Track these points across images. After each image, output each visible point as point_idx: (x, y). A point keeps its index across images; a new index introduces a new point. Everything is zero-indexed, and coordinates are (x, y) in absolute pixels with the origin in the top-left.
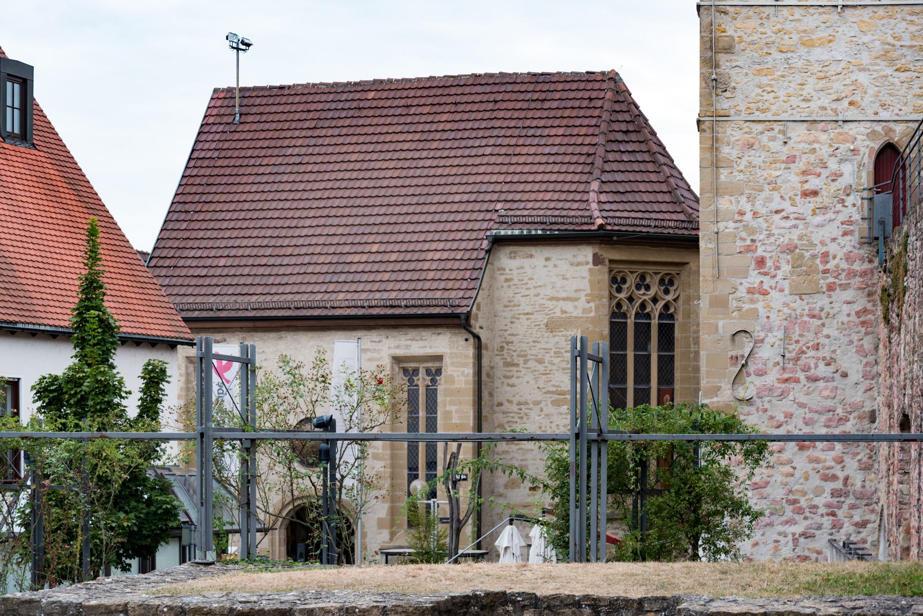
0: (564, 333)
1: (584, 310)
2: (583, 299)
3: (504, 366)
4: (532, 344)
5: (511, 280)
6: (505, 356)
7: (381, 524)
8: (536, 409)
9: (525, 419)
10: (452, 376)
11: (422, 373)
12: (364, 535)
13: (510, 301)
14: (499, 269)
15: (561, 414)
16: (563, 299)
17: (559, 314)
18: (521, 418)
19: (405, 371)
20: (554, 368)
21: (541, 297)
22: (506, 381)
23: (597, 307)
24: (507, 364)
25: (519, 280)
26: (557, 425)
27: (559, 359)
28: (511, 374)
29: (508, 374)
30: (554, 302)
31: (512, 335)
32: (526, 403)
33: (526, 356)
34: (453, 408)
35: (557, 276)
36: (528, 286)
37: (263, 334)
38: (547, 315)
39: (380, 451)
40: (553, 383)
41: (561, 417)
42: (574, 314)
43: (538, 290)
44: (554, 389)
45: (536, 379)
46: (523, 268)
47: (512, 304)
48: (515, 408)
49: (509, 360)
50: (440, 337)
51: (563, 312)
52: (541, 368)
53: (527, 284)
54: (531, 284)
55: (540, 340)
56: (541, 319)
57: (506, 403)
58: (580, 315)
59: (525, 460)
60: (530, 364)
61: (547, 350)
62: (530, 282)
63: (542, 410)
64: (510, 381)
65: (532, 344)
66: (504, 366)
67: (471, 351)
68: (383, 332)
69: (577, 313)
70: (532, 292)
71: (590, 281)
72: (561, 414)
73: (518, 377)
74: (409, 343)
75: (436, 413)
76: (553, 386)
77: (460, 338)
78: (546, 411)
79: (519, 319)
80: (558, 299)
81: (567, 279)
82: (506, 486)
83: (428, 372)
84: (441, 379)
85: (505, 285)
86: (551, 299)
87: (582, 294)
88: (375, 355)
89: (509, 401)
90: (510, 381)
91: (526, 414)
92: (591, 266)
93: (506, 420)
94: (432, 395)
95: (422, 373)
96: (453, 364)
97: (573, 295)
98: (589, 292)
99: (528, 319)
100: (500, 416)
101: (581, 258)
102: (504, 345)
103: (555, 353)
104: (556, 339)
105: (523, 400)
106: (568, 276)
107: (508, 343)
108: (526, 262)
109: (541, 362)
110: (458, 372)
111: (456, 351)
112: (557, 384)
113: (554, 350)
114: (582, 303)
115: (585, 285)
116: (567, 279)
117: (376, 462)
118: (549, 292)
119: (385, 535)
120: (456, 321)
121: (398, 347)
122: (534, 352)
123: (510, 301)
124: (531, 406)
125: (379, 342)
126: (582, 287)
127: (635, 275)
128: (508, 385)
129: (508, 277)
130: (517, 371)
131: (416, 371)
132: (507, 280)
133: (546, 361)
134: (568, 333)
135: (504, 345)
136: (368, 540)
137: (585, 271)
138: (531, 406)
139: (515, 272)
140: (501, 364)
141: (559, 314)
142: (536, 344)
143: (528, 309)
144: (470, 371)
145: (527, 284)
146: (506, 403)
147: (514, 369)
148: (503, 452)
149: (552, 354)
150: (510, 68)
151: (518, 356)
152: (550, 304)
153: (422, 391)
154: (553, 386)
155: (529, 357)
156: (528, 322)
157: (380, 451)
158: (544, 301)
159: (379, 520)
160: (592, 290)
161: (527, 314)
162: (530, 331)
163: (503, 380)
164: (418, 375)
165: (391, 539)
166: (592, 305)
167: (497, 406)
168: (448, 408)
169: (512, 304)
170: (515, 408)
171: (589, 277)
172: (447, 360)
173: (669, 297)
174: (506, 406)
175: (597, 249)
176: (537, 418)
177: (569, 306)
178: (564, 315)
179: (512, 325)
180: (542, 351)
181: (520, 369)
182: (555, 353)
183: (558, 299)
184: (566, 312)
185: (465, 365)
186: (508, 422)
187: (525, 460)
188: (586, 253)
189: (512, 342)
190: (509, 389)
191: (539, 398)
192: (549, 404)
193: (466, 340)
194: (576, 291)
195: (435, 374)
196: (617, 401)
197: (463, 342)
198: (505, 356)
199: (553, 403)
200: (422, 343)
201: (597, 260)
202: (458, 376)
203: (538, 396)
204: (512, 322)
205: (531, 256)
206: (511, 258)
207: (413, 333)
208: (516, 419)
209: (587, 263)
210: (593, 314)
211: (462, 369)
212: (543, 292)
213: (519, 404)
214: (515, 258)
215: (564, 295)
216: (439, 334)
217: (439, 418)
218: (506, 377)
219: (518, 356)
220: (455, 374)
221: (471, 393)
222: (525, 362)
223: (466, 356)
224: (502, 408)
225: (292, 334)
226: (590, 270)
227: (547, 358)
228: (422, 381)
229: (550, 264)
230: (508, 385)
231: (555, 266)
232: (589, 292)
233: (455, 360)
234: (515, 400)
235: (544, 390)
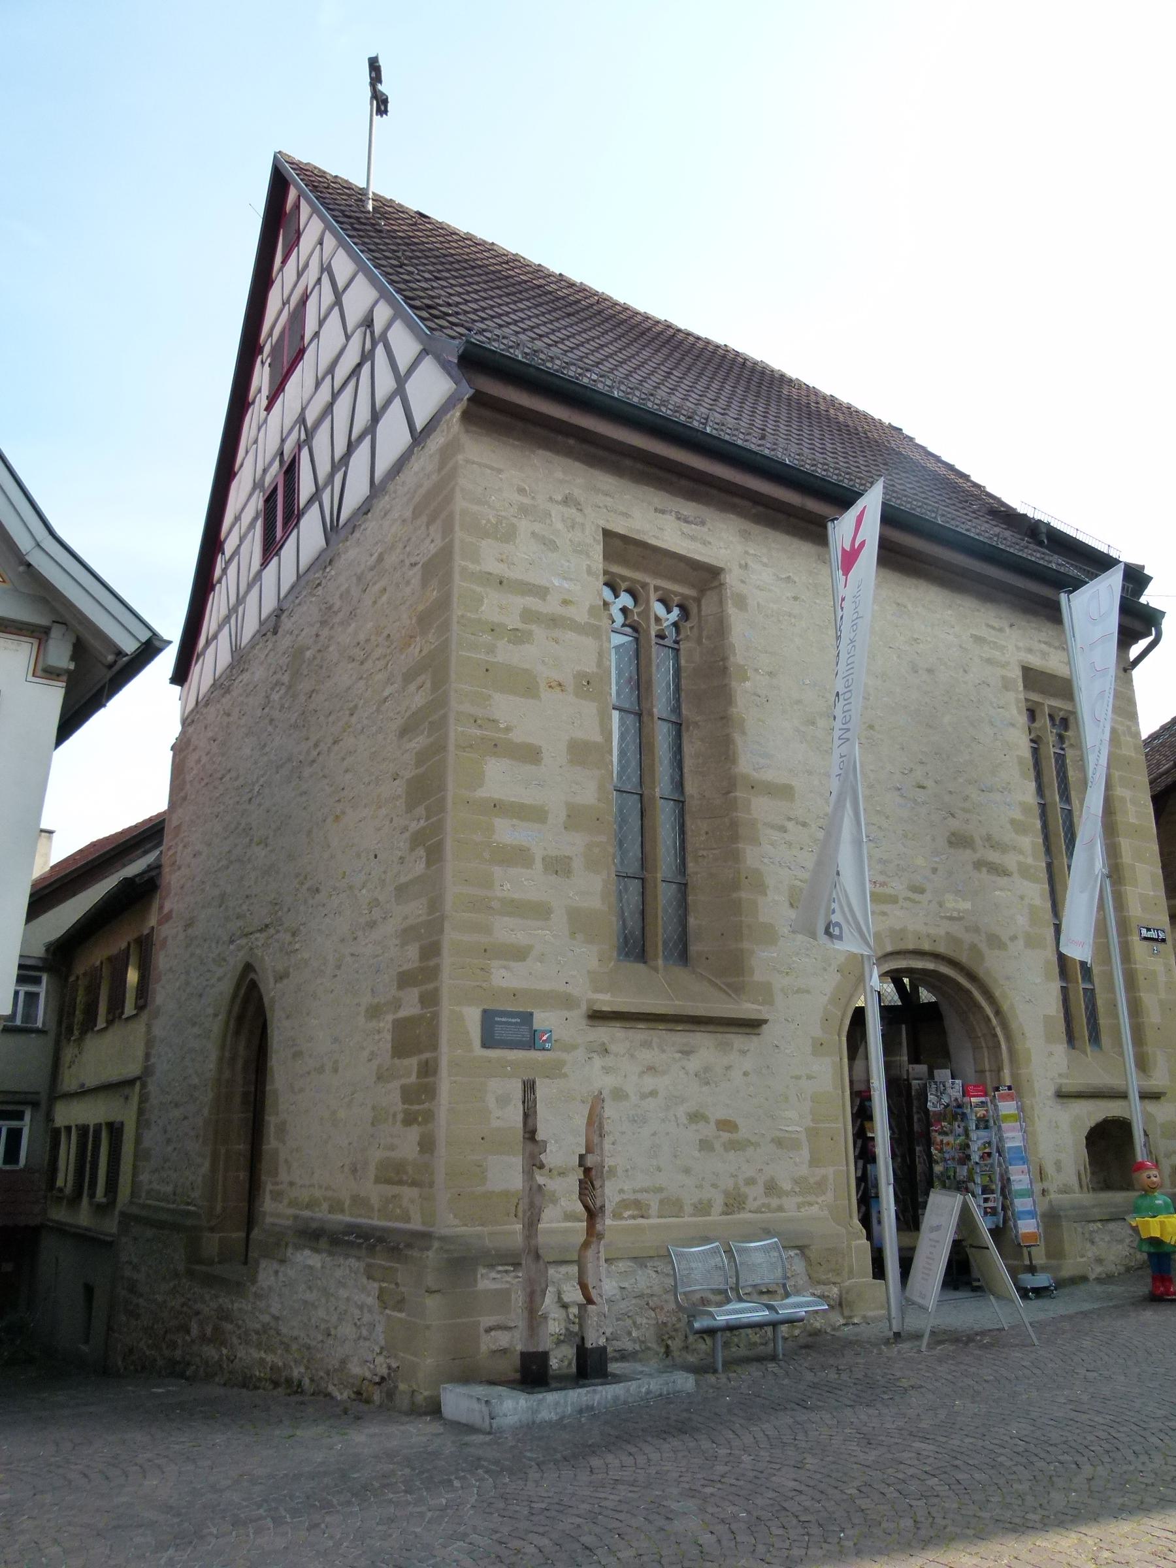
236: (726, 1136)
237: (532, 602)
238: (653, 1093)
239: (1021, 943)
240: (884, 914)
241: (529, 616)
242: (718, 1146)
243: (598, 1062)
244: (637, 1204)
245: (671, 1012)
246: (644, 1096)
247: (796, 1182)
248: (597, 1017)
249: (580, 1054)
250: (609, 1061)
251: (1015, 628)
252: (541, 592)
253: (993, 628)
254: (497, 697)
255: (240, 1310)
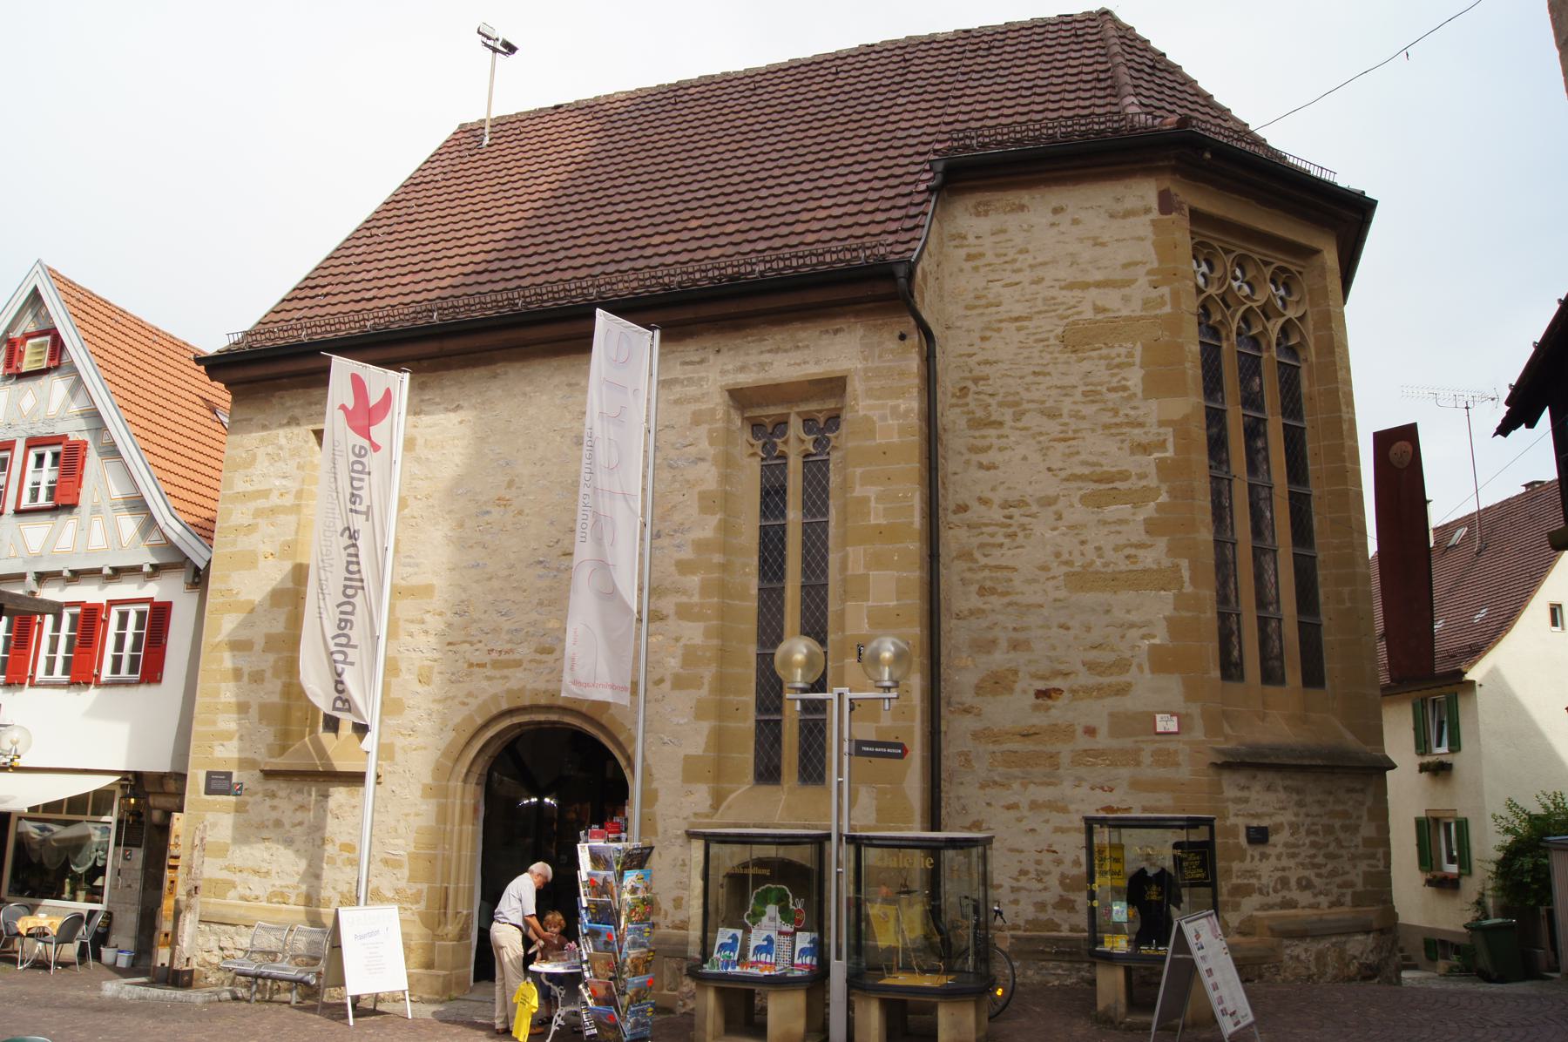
0: (1104, 351)
1: (1146, 304)
2: (1143, 281)
3: (970, 427)
4: (1030, 379)
5: (982, 255)
6: (972, 406)
7: (692, 771)
8: (1049, 513)
9: (1020, 539)
10: (867, 419)
11: (795, 428)
12: (649, 798)
13: (977, 298)
14: (953, 237)
15: (1105, 523)
16: (1098, 285)
17: (1089, 314)
18: (1013, 535)
19: (756, 427)
20: (1084, 425)
21: (1046, 283)
22: (975, 458)
23: (1175, 296)
24: (976, 424)
25: (997, 255)
26: (1098, 549)
27: (1095, 407)
28: (985, 443)
29: (980, 443)
30: (1077, 293)
31: (987, 362)
32: (1022, 503)
33: (1017, 404)
34: (872, 491)
35: (1081, 240)
36: (1018, 265)
37: (460, 372)
38: (1062, 318)
39: (696, 599)
40: (1083, 457)
41: (1105, 530)
42: (1125, 313)
43: (1040, 272)
44: (1086, 471)
45: (1044, 451)
46: (1004, 231)
47: (983, 302)
48: (997, 514)
49: (980, 414)
50: (840, 338)
51: (1098, 310)
52: (1053, 427)
53: (1014, 261)
54: (1024, 260)
55: (1050, 368)
56: (1051, 326)
57: (975, 505)
58: (1138, 313)
59: (1023, 629)
60: (1026, 421)
61: (1066, 390)
62: (1021, 257)
63: (1060, 518)
64: (985, 459)
65: (1030, 379)
66: (970, 427)
67: (913, 363)
68: (710, 342)
69: (1134, 309)
70: (1025, 277)
71: (1156, 245)
72: (1105, 523)
73: (1001, 450)
74: (766, 357)
75: (826, 514)
76: (1085, 463)
77: (886, 335)
78: (1072, 517)
79: (999, 330)
80: (1085, 286)
81: (1103, 245)
82: (979, 689)
83: (809, 422)
84: (845, 441)
85: (968, 266)
86: (1071, 286)
87: (1141, 270)
88: (692, 390)
89: (984, 501)
90: (985, 459)
91: (1023, 527)
92: (1155, 214)
93: (975, 541)
94: (816, 473)
95: (795, 428)
96: (870, 393)
97: (1118, 275)
98: (1156, 265)
99: (1019, 329)
100: (963, 533)
101: (1130, 202)
102: (969, 384)
103: (1084, 394)
104: (1086, 366)
105: (1014, 496)
106: (1105, 238)
107: (976, 381)
108: (1012, 221)
109: (1053, 415)
110: (882, 408)
111: (877, 364)
112: (1092, 459)
113: (1082, 388)
114: (1141, 288)
115: (1147, 253)
116: (1103, 245)
117: (684, 624)
118: (1064, 273)
119: (701, 797)
120: (883, 288)
121: (742, 369)
122: (1036, 395)
123: (977, 298)
124: (1034, 508)
125: (701, 362)
126: (1139, 257)
127: (1232, 256)
128: (981, 466)
129: (973, 251)
130: (999, 437)
131: (781, 424)
132: (969, 257)
133: (1065, 411)
134: (1113, 352)
135: (969, 384)
136: (659, 808)
137: (1142, 226)
138: (1034, 508)
139: (988, 241)
140: (962, 423)
141: (1089, 314)
142: (1040, 379)
143: (1019, 310)
144: (912, 404)
145: (1014, 261)
146: (975, 505)
147: (992, 432)
148: (972, 613)
149: (1078, 397)
150: (923, 30)
151: (1000, 405)
152: (1068, 297)
153: (795, 465)
154: (1085, 463)
155: (1025, 406)
156: (1021, 336)
157: (696, 599)
158: (1054, 292)
159: (688, 760)
160: (1161, 261)
161: (1017, 319)
162: (1026, 353)
163: (967, 456)
164: (783, 433)
165: (715, 807)
166: (1165, 290)
167: (955, 512)
168: (858, 491)
169: (983, 302)
170: (997, 514)
171: (1151, 236)
172: (856, 386)
173: (1291, 313)
174: (977, 512)
175: (1167, 183)
176: (1049, 534)
177: (1111, 299)
178: (1100, 317)
179: (986, 344)
180: (1054, 392)
181: (1005, 431)
182: (1084, 394)
183: (1085, 286)
184: (1105, 310)
185: (901, 393)
186: (982, 546)
187: (1023, 629)
188: (1143, 193)
189: (986, 378)
190: (981, 474)
191: (1052, 492)
192: (1076, 501)
193: (902, 337)
194: (1125, 266)
195: (825, 426)
196: (768, 773)
197: (892, 343)
198: (972, 406)
199: (1083, 499)
200: (797, 356)
201: (1166, 203)
202: (883, 418)
203: (1051, 487)
204: (983, 339)
205: (1022, 208)
206: (978, 214)
207: (777, 336)
208: (1000, 539)
209: (1147, 211)
210: (1167, 309)
211: (891, 403)
212: (1050, 273)
213: (1006, 505)
214: (986, 214)
215: (1099, 276)
216: (836, 332)
217: (832, 524)
218: (973, 449)
219: (1000, 405)
220: (875, 415)
221: (917, 452)
222: (1018, 416)
223: (902, 373)
224: (968, 515)
225: (518, 365)
226: (1154, 223)
227: (1067, 405)
228: (796, 442)
229: (1064, 220)
230: (981, 466)
231: (1075, 222)
232: (1156, 265)
233: (876, 384)
234: (997, 497)
235: (1063, 474)
236: (346, 854)
237: (261, 503)
238: (300, 824)
239: (666, 686)
240: (506, 677)
241: (259, 513)
242: (339, 863)
243: (268, 802)
244: (282, 894)
245: (283, 768)
246: (294, 825)
247: (397, 891)
248: (269, 774)
249: (259, 797)
250: (275, 802)
251: (724, 350)
252: (265, 494)
253: (692, 363)
254: (1437, 516)
255: (1362, 804)
